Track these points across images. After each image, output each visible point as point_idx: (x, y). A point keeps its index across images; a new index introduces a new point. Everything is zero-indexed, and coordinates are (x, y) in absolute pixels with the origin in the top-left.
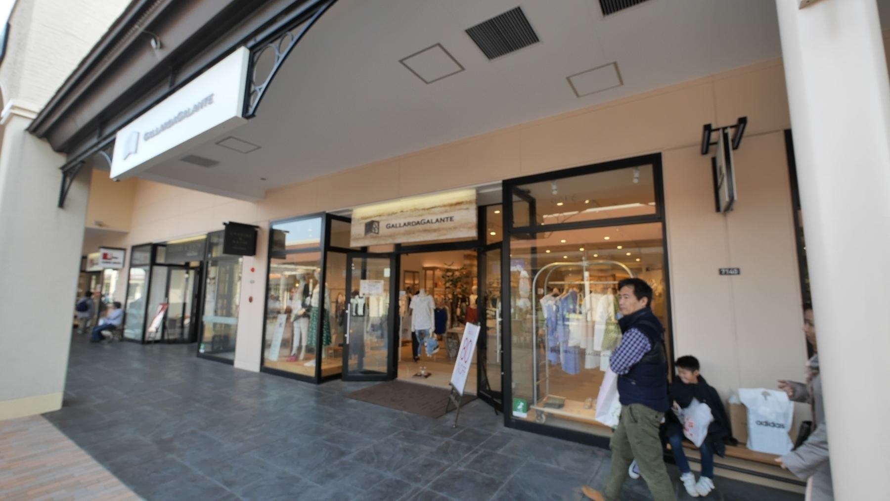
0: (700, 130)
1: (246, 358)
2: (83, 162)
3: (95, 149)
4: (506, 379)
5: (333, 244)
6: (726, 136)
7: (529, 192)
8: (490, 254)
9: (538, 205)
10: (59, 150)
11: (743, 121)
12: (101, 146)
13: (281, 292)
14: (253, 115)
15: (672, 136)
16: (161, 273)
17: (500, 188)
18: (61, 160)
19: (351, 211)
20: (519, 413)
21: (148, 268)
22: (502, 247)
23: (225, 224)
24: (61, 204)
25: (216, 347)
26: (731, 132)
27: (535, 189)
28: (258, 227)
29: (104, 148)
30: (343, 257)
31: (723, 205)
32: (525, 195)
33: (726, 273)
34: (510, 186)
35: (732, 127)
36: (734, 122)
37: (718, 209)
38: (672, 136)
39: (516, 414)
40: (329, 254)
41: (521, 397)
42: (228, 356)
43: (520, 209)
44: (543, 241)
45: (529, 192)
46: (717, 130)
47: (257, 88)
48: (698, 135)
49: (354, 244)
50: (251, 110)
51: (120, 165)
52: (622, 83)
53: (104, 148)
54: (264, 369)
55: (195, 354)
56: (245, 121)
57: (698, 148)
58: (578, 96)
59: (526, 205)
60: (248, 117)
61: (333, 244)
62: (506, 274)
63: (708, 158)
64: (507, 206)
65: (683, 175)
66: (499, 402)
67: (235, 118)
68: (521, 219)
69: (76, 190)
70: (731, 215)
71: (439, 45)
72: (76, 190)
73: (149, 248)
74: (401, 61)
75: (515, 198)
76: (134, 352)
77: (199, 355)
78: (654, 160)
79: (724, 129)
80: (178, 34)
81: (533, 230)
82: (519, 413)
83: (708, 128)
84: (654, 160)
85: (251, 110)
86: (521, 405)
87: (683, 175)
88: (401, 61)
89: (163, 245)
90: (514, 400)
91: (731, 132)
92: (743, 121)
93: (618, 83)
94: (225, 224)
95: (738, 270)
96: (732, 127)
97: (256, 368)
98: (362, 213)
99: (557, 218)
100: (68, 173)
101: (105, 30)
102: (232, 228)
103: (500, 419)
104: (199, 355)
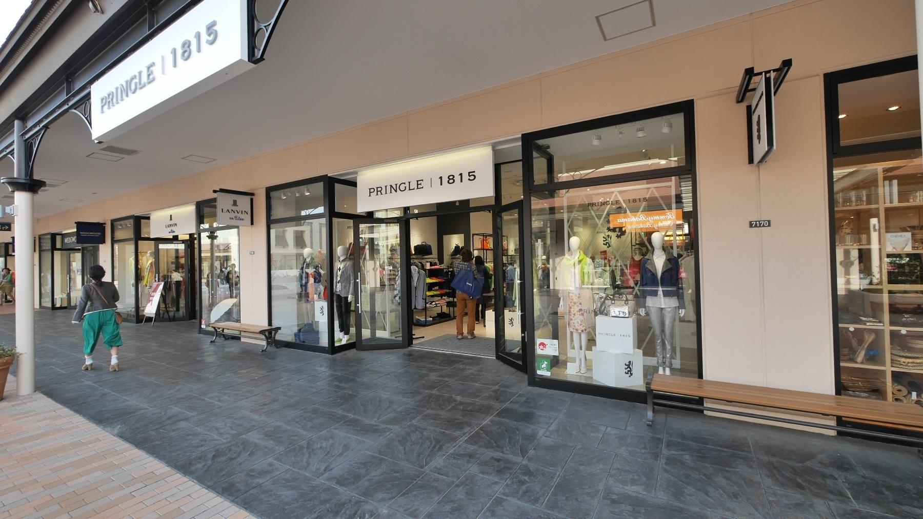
0: (742, 73)
3: (66, 107)
5: (338, 209)
6: (768, 80)
8: (506, 217)
9: (556, 162)
11: (787, 63)
12: (71, 103)
13: (874, 236)
14: (262, 59)
15: (708, 83)
16: (58, 255)
17: (520, 143)
19: (356, 173)
20: (543, 371)
22: (521, 207)
26: (773, 75)
27: (555, 144)
28: (253, 194)
29: (76, 106)
30: (350, 222)
31: (757, 157)
33: (756, 226)
34: (530, 141)
35: (774, 71)
37: (751, 161)
38: (708, 83)
39: (539, 372)
40: (336, 221)
43: (539, 164)
44: (564, 198)
45: (548, 147)
46: (760, 74)
47: (262, 26)
48: (737, 79)
49: (361, 209)
50: (258, 54)
51: (104, 121)
52: (654, 24)
53: (76, 106)
55: (197, 330)
56: (252, 65)
58: (605, 39)
60: (256, 62)
61: (338, 209)
63: (743, 105)
65: (717, 125)
66: (520, 363)
67: (240, 62)
68: (540, 176)
75: (535, 154)
76: (126, 329)
78: (686, 109)
79: (767, 72)
80: (89, 25)
81: (551, 188)
82: (543, 371)
83: (750, 72)
84: (686, 109)
85: (258, 54)
86: (545, 364)
90: (538, 360)
91: (773, 75)
92: (787, 63)
95: (769, 221)
96: (774, 71)
98: (368, 177)
99: (573, 176)
101: (22, 12)
102: (784, 61)
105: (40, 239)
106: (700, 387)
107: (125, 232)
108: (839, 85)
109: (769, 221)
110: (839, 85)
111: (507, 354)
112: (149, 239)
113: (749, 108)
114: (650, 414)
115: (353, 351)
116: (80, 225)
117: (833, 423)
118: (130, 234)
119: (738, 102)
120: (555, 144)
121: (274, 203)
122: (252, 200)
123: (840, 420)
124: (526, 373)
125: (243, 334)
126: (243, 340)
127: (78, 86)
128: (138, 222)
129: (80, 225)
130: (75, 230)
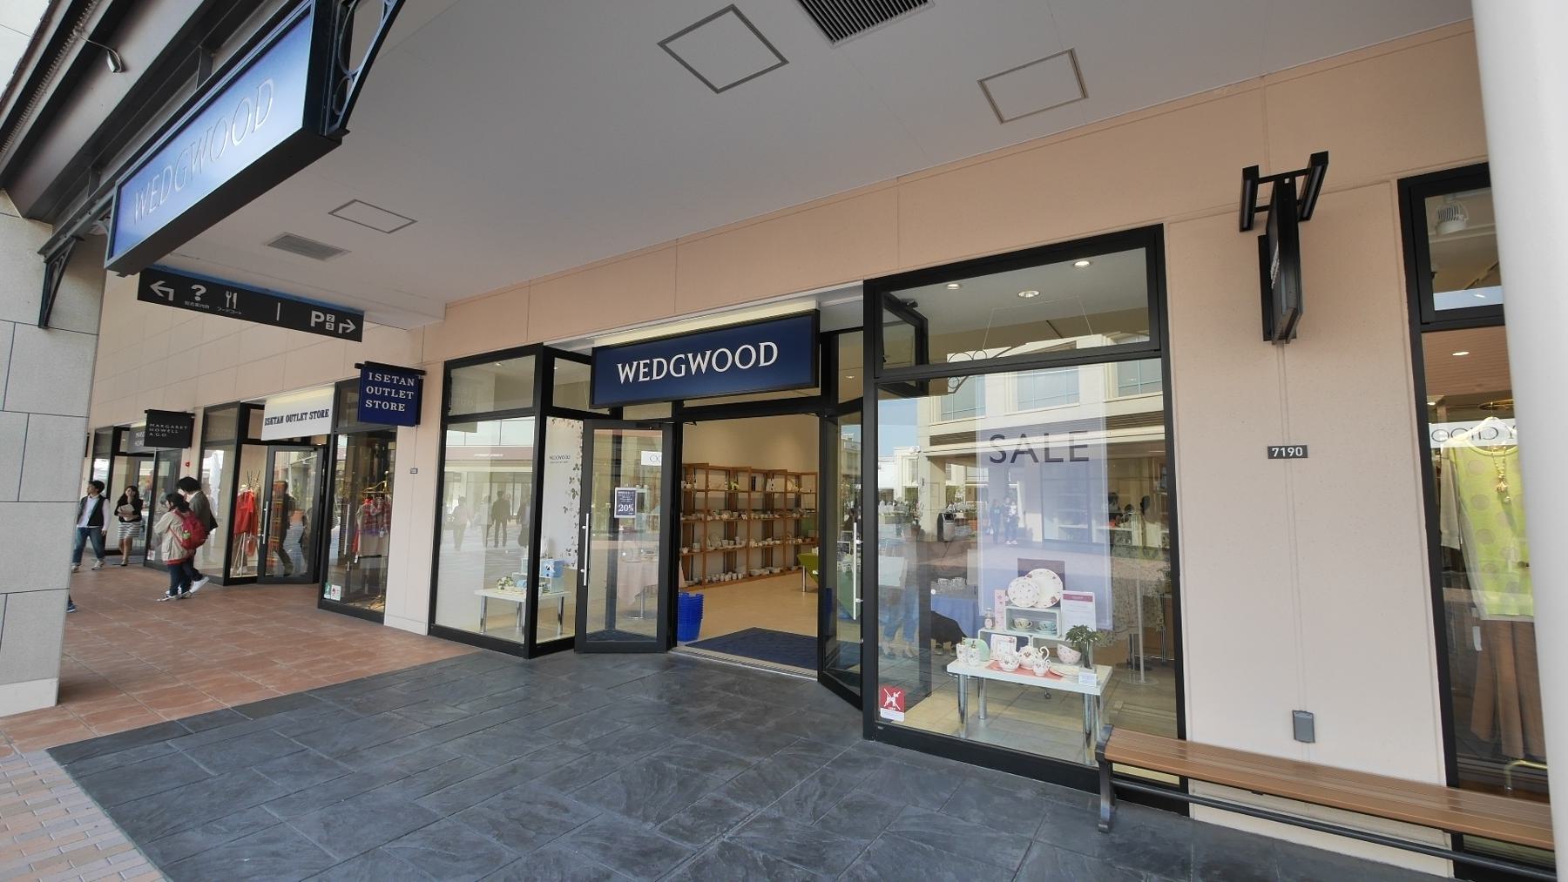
1: (404, 605)
2: (76, 237)
4: (869, 650)
7: (915, 304)
10: (30, 215)
11: (1320, 160)
12: (94, 210)
18: (41, 234)
20: (890, 713)
21: (234, 447)
23: (358, 366)
24: (44, 322)
25: (354, 588)
27: (924, 297)
28: (423, 373)
31: (1282, 322)
32: (907, 311)
33: (1280, 456)
34: (878, 292)
36: (1304, 164)
37: (1268, 335)
39: (884, 713)
40: (245, 447)
41: (894, 685)
42: (376, 607)
43: (897, 337)
45: (915, 304)
52: (1085, 95)
54: (436, 631)
57: (1234, 219)
58: (1002, 121)
59: (908, 330)
61: (251, 436)
62: (1146, 618)
63: (1252, 238)
64: (872, 329)
66: (856, 690)
69: (71, 291)
70: (1291, 350)
71: (733, 8)
72: (71, 291)
73: (235, 411)
74: (662, 44)
75: (888, 316)
77: (325, 605)
78: (1150, 239)
84: (1150, 239)
87: (1211, 273)
88: (662, 44)
89: (127, 429)
90: (883, 689)
92: (1320, 160)
93: (1078, 95)
94: (358, 366)
95: (1305, 448)
97: (422, 629)
100: (57, 262)
103: (857, 716)
104: (325, 605)
105: (97, 435)
106: (1182, 754)
107: (227, 428)
108: (1428, 200)
109: (1305, 448)
110: (1428, 200)
111: (842, 675)
112: (258, 442)
113: (1264, 244)
114: (1105, 805)
115: (569, 654)
116: (153, 415)
117: (1445, 841)
118: (231, 433)
119: (1243, 229)
120: (924, 297)
121: (456, 389)
122: (421, 381)
123: (1457, 838)
124: (59, 701)
125: (1195, 788)
126: (1198, 813)
127: (104, 181)
128: (247, 412)
129: (153, 415)
130: (144, 424)
